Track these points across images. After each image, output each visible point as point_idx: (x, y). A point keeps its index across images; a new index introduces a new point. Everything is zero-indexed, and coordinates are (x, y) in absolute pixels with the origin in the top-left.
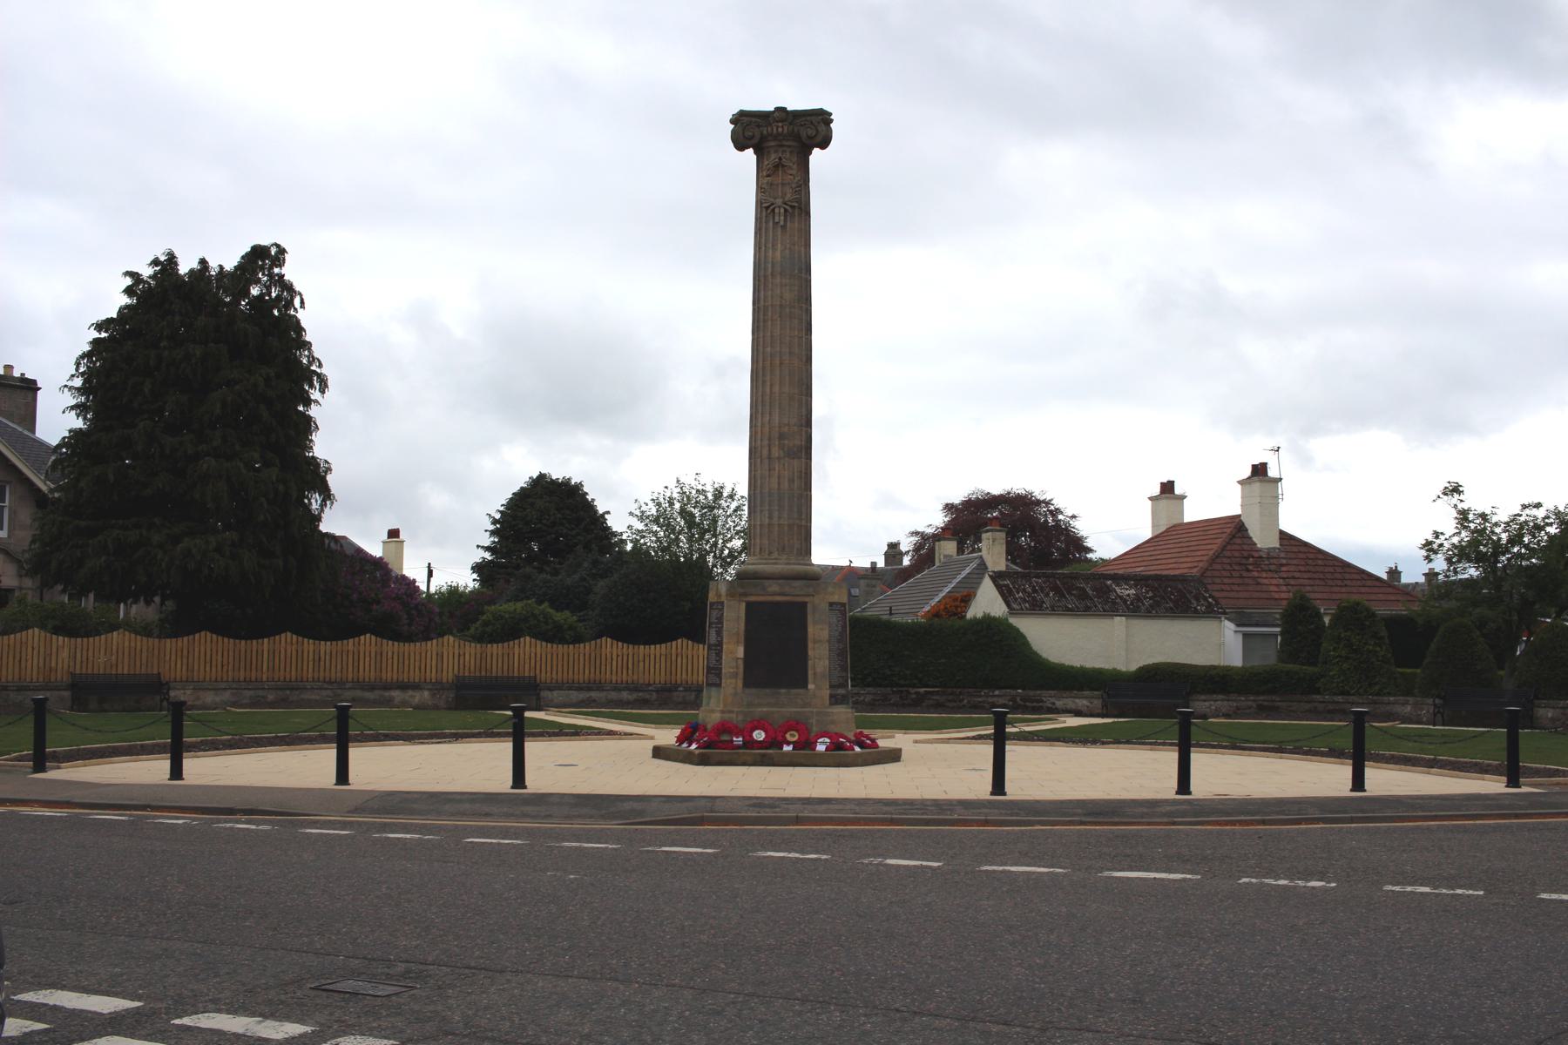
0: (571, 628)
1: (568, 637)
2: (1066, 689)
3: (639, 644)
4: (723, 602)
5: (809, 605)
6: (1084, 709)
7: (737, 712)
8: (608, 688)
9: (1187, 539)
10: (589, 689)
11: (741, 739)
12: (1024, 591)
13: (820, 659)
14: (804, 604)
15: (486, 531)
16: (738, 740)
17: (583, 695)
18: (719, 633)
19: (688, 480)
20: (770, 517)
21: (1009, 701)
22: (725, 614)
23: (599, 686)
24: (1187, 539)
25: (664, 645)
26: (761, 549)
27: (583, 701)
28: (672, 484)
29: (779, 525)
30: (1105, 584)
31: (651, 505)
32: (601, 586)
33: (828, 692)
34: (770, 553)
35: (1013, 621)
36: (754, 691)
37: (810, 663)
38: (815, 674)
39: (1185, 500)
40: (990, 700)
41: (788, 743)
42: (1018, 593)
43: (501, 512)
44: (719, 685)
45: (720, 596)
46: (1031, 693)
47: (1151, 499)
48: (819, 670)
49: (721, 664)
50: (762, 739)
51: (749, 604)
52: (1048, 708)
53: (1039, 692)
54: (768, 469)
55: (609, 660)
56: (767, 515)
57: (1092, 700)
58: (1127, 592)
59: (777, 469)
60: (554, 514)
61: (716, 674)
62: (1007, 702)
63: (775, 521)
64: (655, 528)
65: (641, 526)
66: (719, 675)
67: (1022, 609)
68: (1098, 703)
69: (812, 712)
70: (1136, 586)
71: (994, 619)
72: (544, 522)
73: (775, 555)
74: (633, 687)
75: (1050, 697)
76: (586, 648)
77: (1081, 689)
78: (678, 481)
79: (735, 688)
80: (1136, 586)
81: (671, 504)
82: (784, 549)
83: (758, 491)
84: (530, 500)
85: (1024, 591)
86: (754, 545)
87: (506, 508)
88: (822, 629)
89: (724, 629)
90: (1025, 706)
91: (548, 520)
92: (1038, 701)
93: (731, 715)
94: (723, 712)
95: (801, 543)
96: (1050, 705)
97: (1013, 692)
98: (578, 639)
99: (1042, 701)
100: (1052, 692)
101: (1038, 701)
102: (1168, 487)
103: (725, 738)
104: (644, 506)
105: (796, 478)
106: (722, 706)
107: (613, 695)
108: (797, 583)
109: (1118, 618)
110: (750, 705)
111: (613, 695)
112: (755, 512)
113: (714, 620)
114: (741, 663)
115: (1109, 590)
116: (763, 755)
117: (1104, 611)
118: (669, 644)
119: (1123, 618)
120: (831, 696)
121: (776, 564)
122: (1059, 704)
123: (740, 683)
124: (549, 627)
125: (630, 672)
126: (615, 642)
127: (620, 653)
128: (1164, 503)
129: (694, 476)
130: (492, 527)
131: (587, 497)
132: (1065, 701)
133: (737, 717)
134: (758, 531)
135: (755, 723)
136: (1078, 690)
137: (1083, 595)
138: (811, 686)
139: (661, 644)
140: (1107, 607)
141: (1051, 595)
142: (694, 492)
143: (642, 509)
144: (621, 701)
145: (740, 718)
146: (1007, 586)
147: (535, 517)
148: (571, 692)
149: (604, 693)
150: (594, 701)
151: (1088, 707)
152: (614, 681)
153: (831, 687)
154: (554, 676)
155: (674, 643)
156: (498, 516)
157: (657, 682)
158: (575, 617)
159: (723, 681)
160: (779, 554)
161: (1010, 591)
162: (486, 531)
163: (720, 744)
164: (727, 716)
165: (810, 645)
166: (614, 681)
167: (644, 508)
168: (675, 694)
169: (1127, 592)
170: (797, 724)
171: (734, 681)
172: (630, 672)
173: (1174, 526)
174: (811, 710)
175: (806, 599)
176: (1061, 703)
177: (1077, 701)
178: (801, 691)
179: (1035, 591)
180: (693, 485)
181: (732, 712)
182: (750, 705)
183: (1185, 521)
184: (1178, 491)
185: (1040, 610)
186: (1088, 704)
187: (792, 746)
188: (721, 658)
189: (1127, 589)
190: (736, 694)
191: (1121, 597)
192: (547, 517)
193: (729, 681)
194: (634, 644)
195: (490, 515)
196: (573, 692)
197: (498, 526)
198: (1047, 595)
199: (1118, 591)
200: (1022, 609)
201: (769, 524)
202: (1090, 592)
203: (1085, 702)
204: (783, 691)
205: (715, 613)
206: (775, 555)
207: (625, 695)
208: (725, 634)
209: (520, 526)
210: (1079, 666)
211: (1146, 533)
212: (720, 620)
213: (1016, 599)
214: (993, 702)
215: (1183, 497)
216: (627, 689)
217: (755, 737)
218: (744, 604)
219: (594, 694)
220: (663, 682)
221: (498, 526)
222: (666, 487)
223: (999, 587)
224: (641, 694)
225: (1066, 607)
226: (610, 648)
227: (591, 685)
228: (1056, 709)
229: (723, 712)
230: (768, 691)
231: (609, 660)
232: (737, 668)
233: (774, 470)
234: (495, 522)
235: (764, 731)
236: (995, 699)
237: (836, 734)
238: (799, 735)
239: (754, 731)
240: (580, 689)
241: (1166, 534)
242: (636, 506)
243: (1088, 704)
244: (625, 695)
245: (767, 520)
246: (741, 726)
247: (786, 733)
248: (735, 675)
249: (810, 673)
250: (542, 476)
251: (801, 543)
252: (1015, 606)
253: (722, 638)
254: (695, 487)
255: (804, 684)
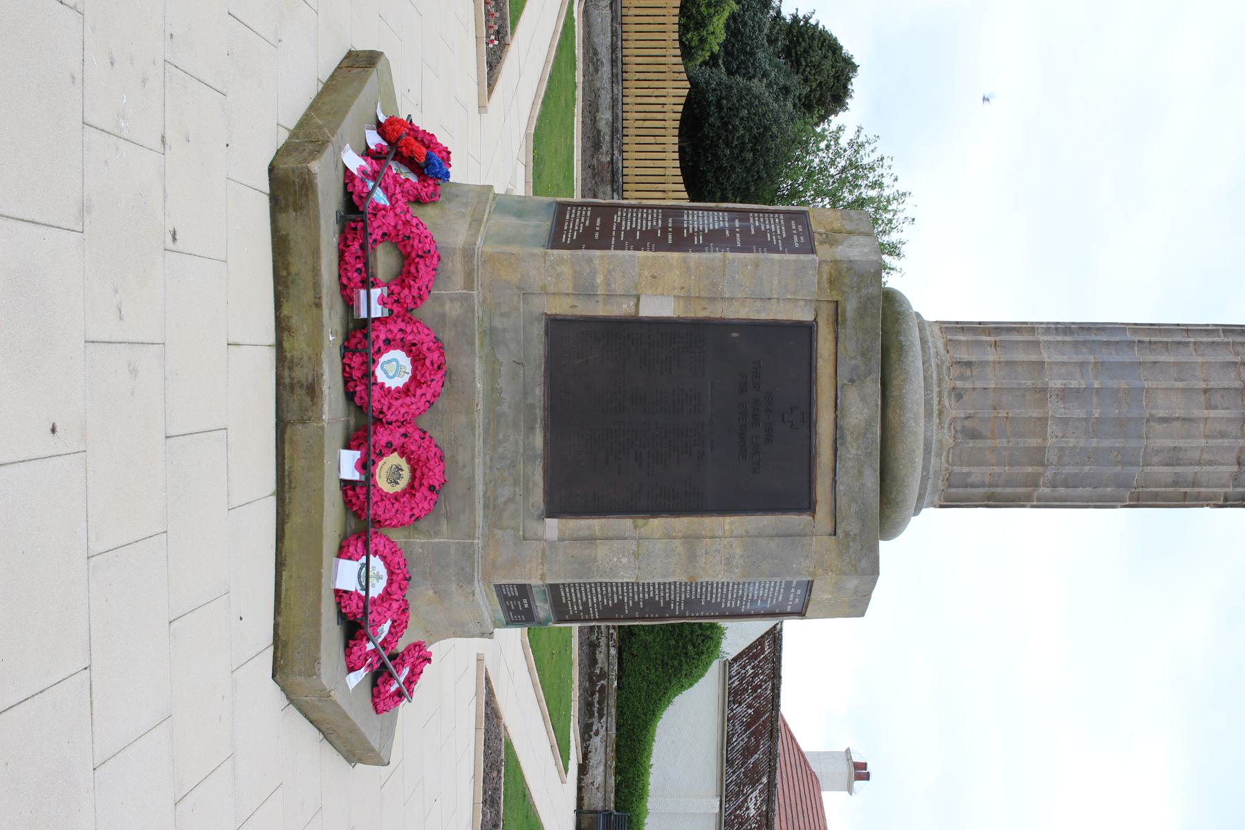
0: (702, 41)
1: (689, 36)
2: (618, 749)
3: (680, 136)
4: (813, 251)
5: (805, 518)
6: (588, 779)
7: (466, 299)
8: (615, 91)
9: (805, 810)
10: (613, 62)
11: (377, 311)
12: (755, 675)
13: (636, 555)
14: (808, 506)
15: (797, 9)
16: (373, 304)
17: (604, 55)
18: (715, 239)
19: (905, 209)
20: (1065, 394)
21: (601, 669)
22: (776, 256)
23: (618, 77)
24: (805, 810)
25: (679, 172)
26: (969, 364)
27: (596, 53)
28: (901, 187)
29: (1043, 421)
30: (763, 775)
31: (874, 157)
32: (758, 86)
33: (535, 580)
34: (958, 394)
35: (713, 673)
36: (538, 349)
37: (624, 524)
38: (592, 539)
39: (847, 793)
40: (603, 641)
41: (365, 466)
42: (753, 668)
43: (817, 24)
44: (555, 241)
45: (831, 238)
46: (612, 701)
47: (848, 751)
48: (602, 551)
49: (619, 246)
50: (381, 376)
51: (806, 331)
52: (592, 724)
53: (613, 711)
54: (1212, 384)
55: (657, 92)
56: (1074, 384)
57: (602, 790)
58: (752, 806)
59: (1212, 413)
60: (816, 80)
61: (589, 231)
62: (600, 665)
63: (1055, 408)
64: (842, 163)
65: (843, 142)
66: (586, 240)
67: (730, 679)
68: (596, 800)
69: (472, 536)
70: (760, 815)
71: (718, 644)
72: (808, 69)
73: (954, 411)
74: (617, 130)
75: (606, 728)
76: (673, 53)
77: (619, 771)
78: (904, 194)
79: (545, 292)
80: (760, 815)
81: (874, 185)
82: (974, 435)
83: (1137, 355)
84: (830, 54)
85: (755, 675)
86: (979, 343)
87: (820, 32)
88: (729, 561)
89: (730, 255)
90: (593, 694)
91: (810, 73)
92: (600, 711)
93: (459, 280)
94: (468, 253)
95: (982, 485)
96: (595, 728)
97: (613, 675)
98: (687, 52)
99: (601, 717)
100: (613, 732)
101: (600, 711)
102: (861, 772)
103: (384, 261)
104: (872, 147)
105: (1178, 469)
106: (488, 250)
107: (605, 99)
108: (871, 480)
109: (718, 803)
110: (493, 336)
111: (605, 99)
112: (1076, 344)
113: (754, 223)
114: (622, 309)
115: (754, 783)
116: (313, 390)
117: (727, 786)
118: (681, 179)
119: (718, 810)
120: (524, 590)
121: (929, 415)
122: (596, 742)
123: (562, 307)
124: (703, 9)
125: (640, 124)
126: (683, 100)
127: (666, 108)
128: (844, 770)
129: (911, 216)
130: (801, 16)
131: (833, 116)
132: (601, 751)
133: (452, 299)
134: (1020, 356)
135: (435, 356)
136: (616, 767)
137: (748, 751)
138: (553, 527)
139: (681, 167)
140: (732, 787)
141: (750, 711)
142: (889, 216)
143: (867, 145)
144: (598, 111)
145: (453, 310)
146: (763, 651)
147: (813, 59)
148: (610, 35)
149: (608, 86)
150: (597, 70)
151: (593, 783)
152: (626, 100)
153: (554, 589)
154: (633, 12)
155: (682, 187)
156: (812, 21)
157: (626, 163)
158: (717, 48)
159: (565, 253)
160: (954, 420)
161: (755, 656)
162: (797, 9)
163: (355, 247)
164: (454, 267)
165: (681, 524)
166: (626, 100)
167: (868, 148)
168: (609, 189)
169: (752, 806)
170: (432, 488)
171: (567, 285)
172: (640, 124)
173: (818, 782)
174: (479, 533)
175: (823, 508)
176: (599, 744)
177: (602, 768)
178: (538, 496)
179: (755, 690)
180: (899, 214)
181: (469, 282)
182: (493, 336)
183: (822, 792)
184: (858, 784)
185: (729, 702)
186: (596, 785)
187: (356, 476)
188: (637, 249)
189: (755, 805)
190: (526, 295)
191: (745, 801)
192: (813, 72)
193: (566, 269)
194: (680, 129)
195: (814, 13)
196: (609, 39)
197: (802, 23)
198: (749, 706)
199: (753, 795)
200: (730, 678)
201: (1044, 390)
202: (752, 760)
203: (599, 780)
204: (538, 440)
205: (775, 226)
206: (954, 411)
207: (605, 116)
208: (713, 257)
209: (803, 44)
210: (646, 821)
211: (804, 748)
212: (756, 242)
213: (744, 667)
214: (598, 645)
215: (850, 790)
216: (615, 118)
217: (385, 357)
218: (808, 317)
219: (606, 69)
220: (626, 171)
221: (802, 23)
222: (896, 179)
223: (761, 640)
224: (608, 138)
225: (734, 735)
226: (675, 93)
227: (619, 49)
228: (590, 737)
229: (468, 253)
230: (538, 392)
231: (657, 92)
232: (610, 296)
233: (1210, 406)
234: (806, 19)
235: (407, 386)
236: (603, 648)
237: (404, 610)
238: (396, 497)
239: (409, 353)
240: (613, 48)
241: (809, 772)
242: (871, 137)
243: (596, 785)
244: (605, 116)
245: (1057, 384)
246: (425, 312)
247: (402, 455)
248: (587, 293)
249: (596, 524)
250: (854, 68)
251: (982, 485)
252: (735, 667)
253: (699, 249)
254: (896, 217)
255: (555, 508)
